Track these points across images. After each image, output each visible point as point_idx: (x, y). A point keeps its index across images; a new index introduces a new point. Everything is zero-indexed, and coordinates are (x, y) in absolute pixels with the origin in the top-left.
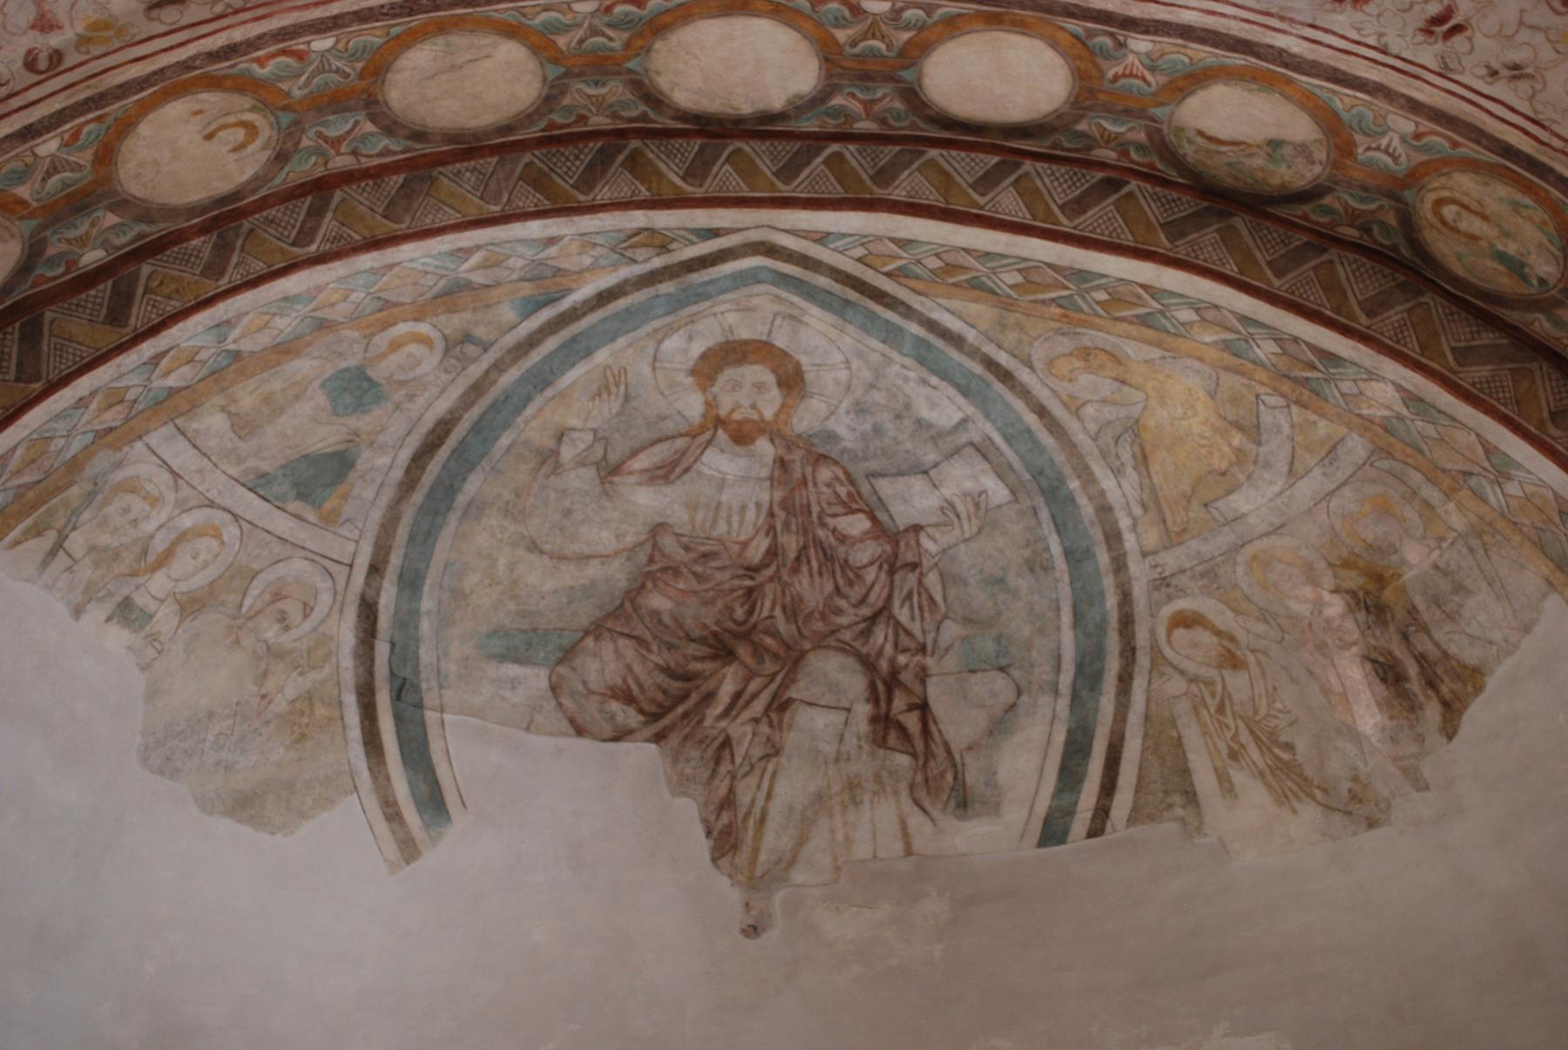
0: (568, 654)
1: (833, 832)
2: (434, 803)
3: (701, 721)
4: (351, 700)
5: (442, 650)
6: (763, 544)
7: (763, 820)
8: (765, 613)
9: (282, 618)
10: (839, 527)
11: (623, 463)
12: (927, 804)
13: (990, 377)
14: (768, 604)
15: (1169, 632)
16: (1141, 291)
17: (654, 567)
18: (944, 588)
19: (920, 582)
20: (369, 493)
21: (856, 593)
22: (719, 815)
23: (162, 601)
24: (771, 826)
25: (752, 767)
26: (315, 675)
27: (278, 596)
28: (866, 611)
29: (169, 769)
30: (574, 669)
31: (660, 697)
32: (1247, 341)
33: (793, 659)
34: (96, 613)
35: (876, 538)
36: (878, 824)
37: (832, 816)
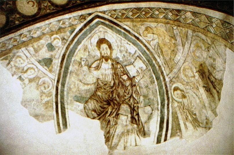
0: (86, 102)
1: (124, 140)
2: (65, 125)
3: (106, 116)
4: (54, 104)
5: (68, 99)
6: (113, 82)
7: (113, 137)
8: (114, 96)
9: (45, 87)
10: (123, 78)
11: (91, 65)
12: (139, 135)
13: (136, 39)
14: (115, 95)
15: (174, 92)
16: (149, 9)
17: (98, 87)
18: (140, 89)
19: (136, 88)
20: (56, 67)
21: (127, 92)
22: (107, 135)
23: (26, 78)
24: (115, 137)
25: (113, 126)
26: (49, 98)
27: (44, 83)
28: (129, 96)
29: (25, 106)
30: (87, 105)
31: (100, 112)
32: (167, 15)
33: (119, 105)
34: (16, 77)
35: (129, 80)
36: (132, 138)
37: (124, 137)
